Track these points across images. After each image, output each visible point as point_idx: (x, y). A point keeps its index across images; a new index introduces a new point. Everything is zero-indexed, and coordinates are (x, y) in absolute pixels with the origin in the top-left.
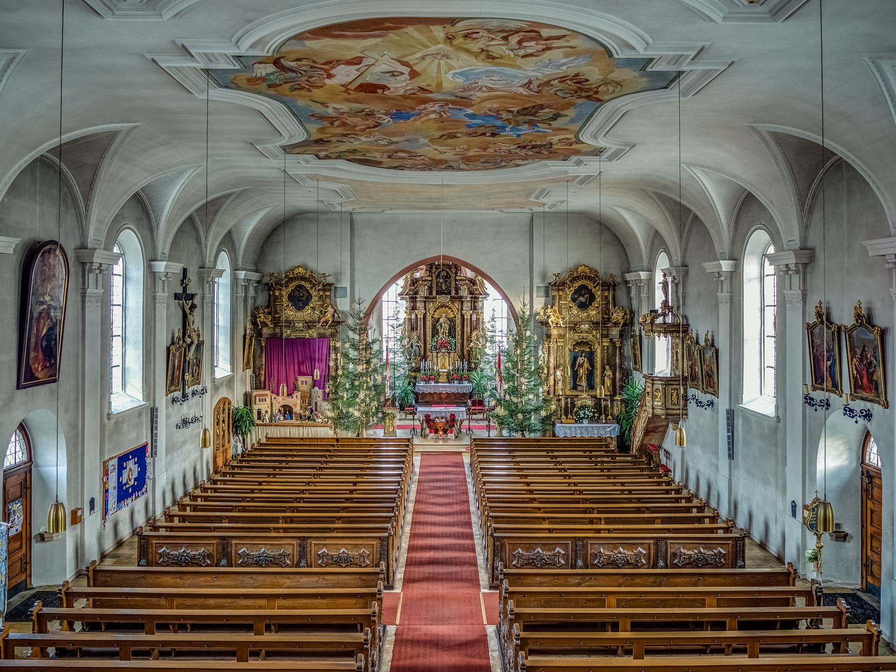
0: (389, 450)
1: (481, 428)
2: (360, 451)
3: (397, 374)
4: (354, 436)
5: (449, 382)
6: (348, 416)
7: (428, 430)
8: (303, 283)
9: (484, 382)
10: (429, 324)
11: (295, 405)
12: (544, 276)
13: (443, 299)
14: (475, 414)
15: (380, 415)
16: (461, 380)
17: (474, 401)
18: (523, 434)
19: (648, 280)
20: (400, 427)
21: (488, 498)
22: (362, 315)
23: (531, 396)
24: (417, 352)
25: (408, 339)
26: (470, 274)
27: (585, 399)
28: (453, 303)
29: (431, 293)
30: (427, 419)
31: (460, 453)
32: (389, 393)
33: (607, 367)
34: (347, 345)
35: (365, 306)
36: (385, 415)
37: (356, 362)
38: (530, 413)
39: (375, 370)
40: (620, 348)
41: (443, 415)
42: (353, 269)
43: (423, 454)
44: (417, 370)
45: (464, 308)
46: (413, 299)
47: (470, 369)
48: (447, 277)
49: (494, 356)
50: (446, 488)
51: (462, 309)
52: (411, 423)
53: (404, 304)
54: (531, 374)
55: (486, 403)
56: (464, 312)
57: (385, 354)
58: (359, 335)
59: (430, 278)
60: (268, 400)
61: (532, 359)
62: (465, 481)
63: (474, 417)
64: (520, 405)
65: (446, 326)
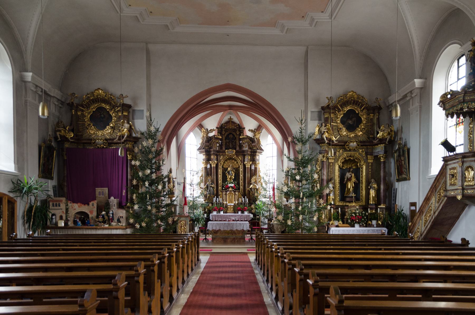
5: (235, 213)
8: (103, 105)
10: (220, 171)
11: (91, 212)
12: (317, 102)
13: (231, 152)
19: (421, 88)
27: (354, 208)
28: (237, 156)
31: (246, 254)
33: (373, 180)
40: (384, 162)
51: (244, 161)
53: (202, 157)
60: (63, 206)
62: (253, 272)
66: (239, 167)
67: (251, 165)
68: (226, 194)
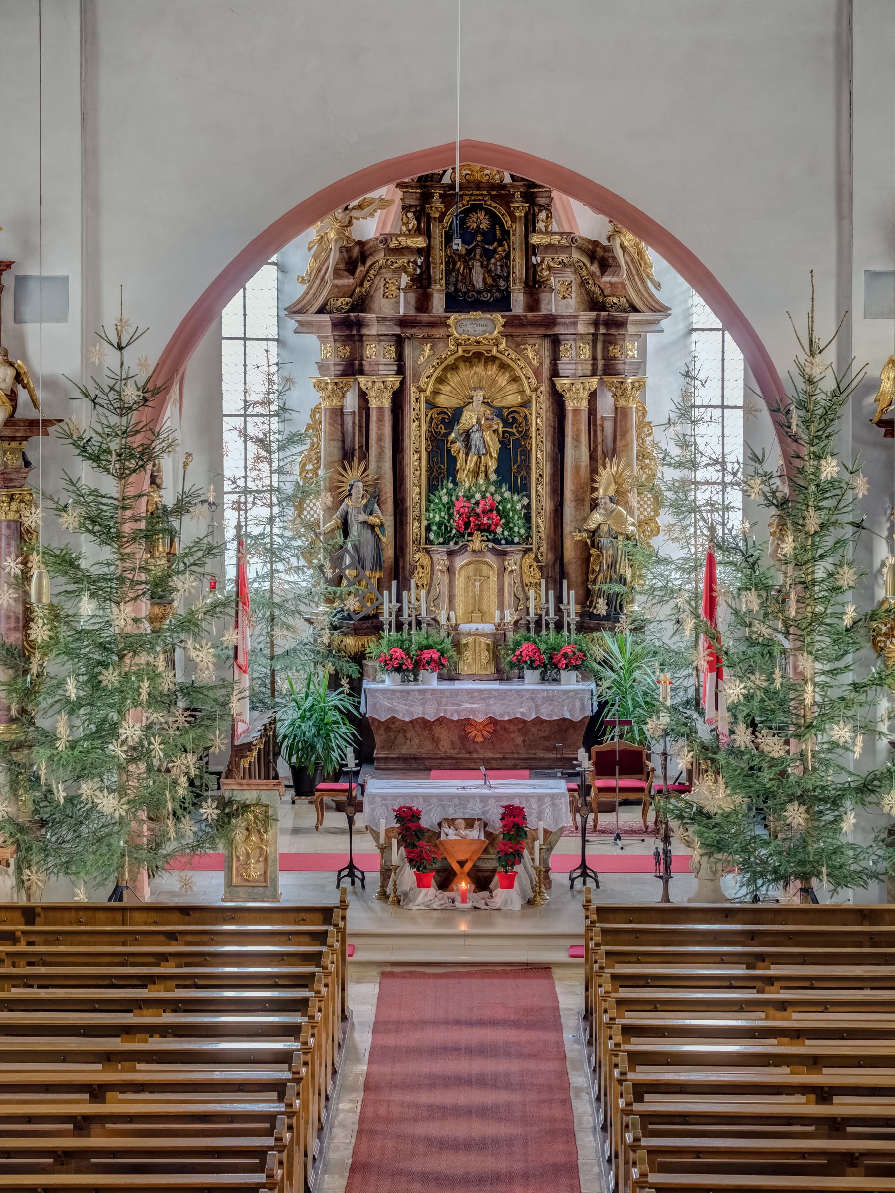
0: (252, 954)
1: (633, 866)
2: (125, 959)
3: (284, 643)
4: (102, 897)
5: (500, 675)
6: (75, 812)
7: (408, 876)
9: (647, 675)
10: (416, 434)
13: (478, 327)
14: (609, 808)
15: (209, 811)
16: (550, 666)
17: (606, 756)
18: (807, 891)
20: (292, 863)
21: (653, 1152)
22: (131, 394)
23: (841, 732)
24: (368, 552)
25: (327, 498)
26: (587, 223)
29: (423, 304)
30: (408, 823)
31: (544, 970)
32: (248, 724)
34: (70, 520)
35: (143, 358)
36: (229, 811)
37: (107, 589)
38: (836, 802)
39: (189, 624)
41: (474, 810)
42: (91, 200)
43: (391, 972)
44: (370, 624)
45: (565, 367)
46: (349, 328)
47: (589, 623)
48: (496, 234)
49: (687, 567)
50: (483, 1112)
51: (555, 373)
52: (338, 845)
53: (319, 348)
54: (844, 638)
55: (655, 763)
56: (562, 383)
57: (230, 557)
58: (121, 476)
59: (419, 242)
61: (847, 577)
62: (560, 1090)
63: (606, 820)
64: (794, 770)
65: (489, 441)
66: (526, 404)
67: (593, 395)
68: (450, 570)
